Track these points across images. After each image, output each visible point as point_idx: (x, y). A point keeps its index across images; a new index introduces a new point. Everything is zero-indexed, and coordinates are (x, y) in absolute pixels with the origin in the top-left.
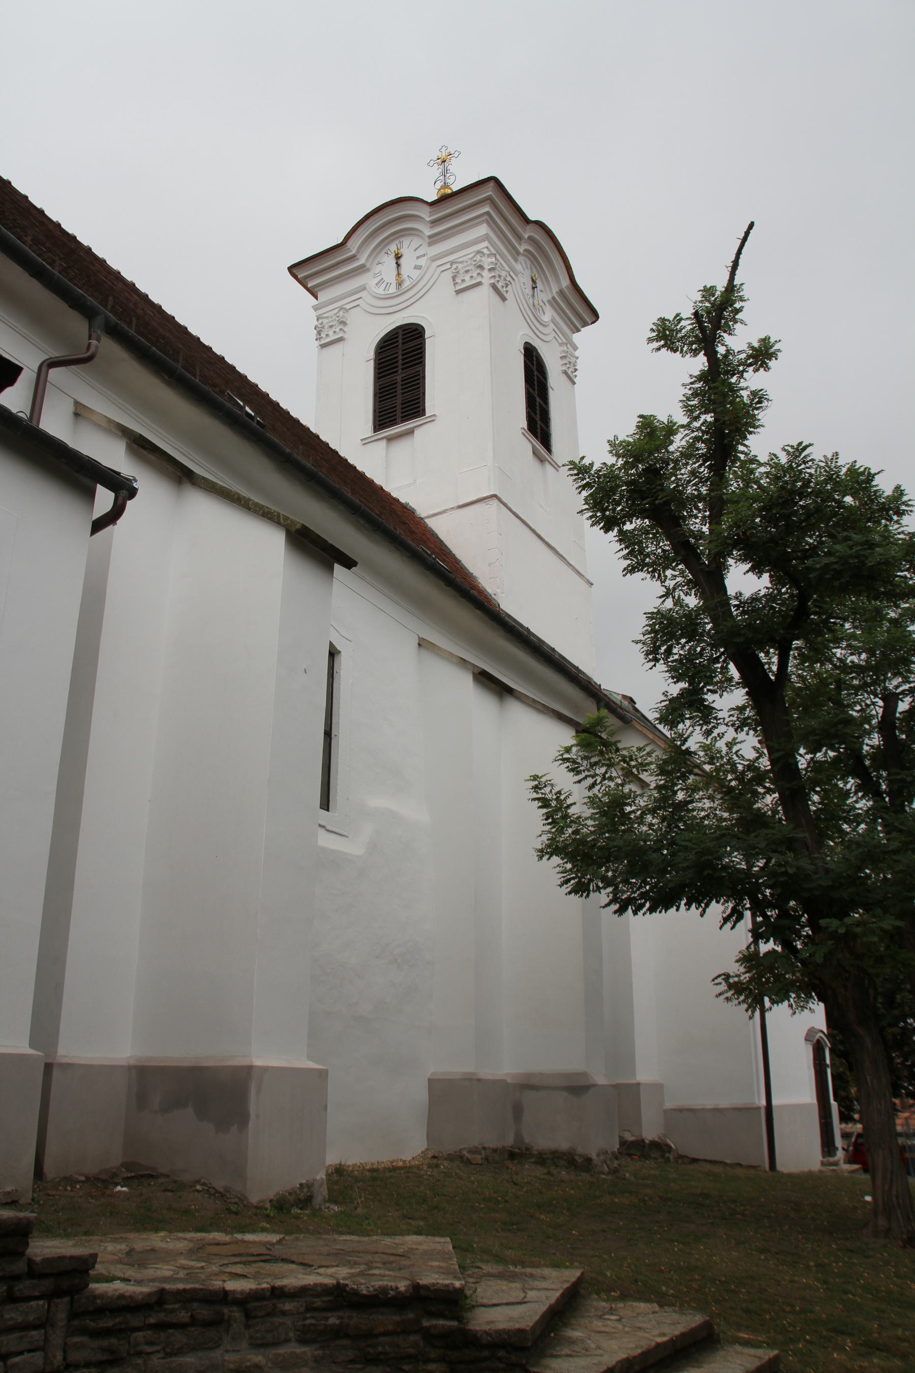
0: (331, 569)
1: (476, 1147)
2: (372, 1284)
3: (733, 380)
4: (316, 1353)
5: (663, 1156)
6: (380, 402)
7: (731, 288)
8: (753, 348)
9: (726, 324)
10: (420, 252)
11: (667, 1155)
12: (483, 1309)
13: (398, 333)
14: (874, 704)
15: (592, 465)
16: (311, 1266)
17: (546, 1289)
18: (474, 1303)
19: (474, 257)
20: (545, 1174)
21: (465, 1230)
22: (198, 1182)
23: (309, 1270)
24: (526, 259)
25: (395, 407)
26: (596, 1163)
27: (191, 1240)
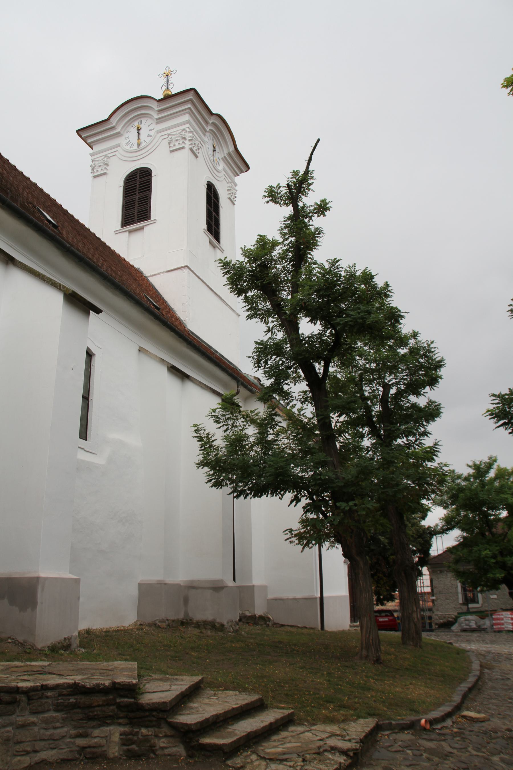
0: (88, 314)
1: (163, 619)
2: (92, 682)
3: (306, 220)
4: (63, 716)
5: (265, 624)
6: (126, 210)
7: (307, 172)
8: (317, 204)
9: (304, 190)
10: (151, 127)
11: (268, 623)
12: (148, 694)
13: (137, 172)
14: (378, 389)
15: (231, 261)
16: (63, 675)
17: (182, 685)
18: (143, 691)
19: (181, 132)
20: (199, 633)
21: (150, 660)
22: (9, 638)
23: (62, 677)
24: (210, 134)
25: (134, 214)
26: (226, 626)
27: (3, 666)
